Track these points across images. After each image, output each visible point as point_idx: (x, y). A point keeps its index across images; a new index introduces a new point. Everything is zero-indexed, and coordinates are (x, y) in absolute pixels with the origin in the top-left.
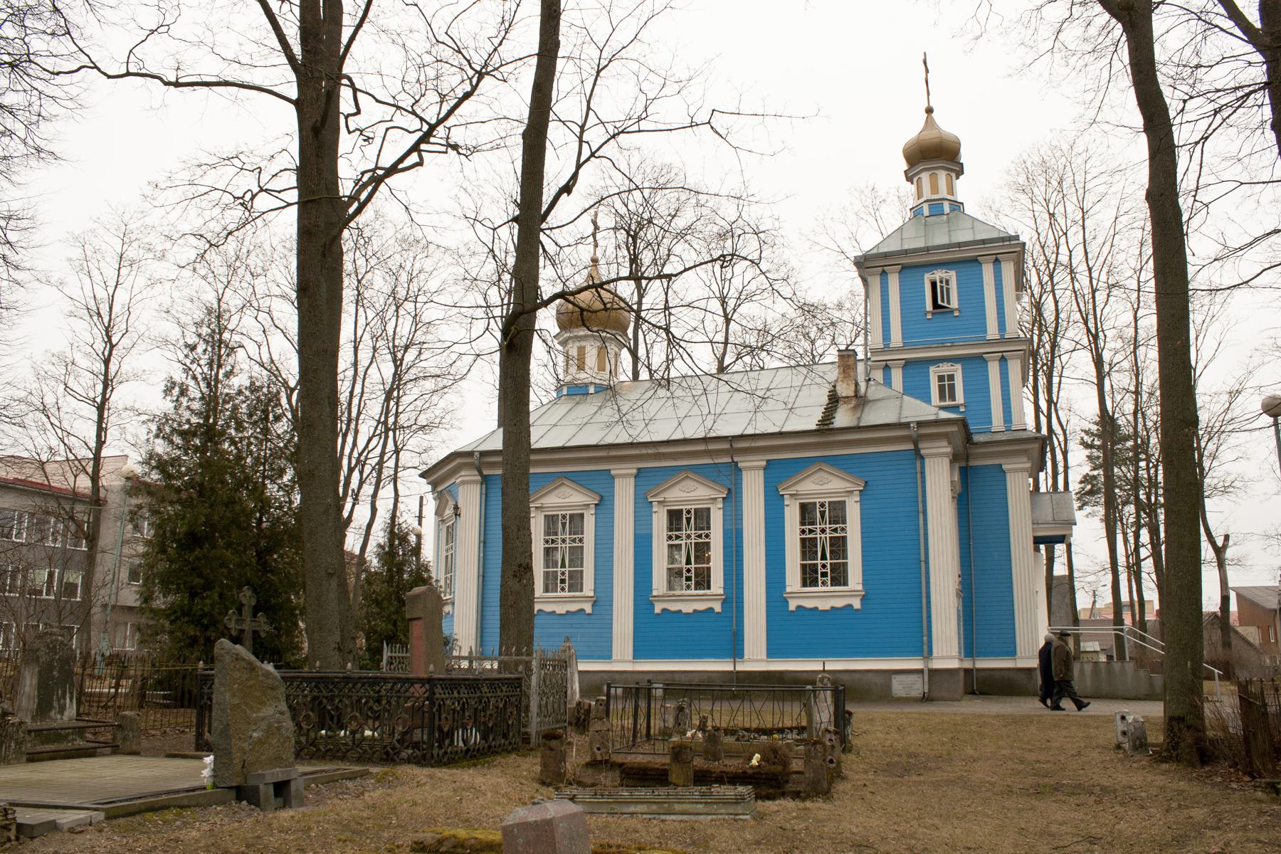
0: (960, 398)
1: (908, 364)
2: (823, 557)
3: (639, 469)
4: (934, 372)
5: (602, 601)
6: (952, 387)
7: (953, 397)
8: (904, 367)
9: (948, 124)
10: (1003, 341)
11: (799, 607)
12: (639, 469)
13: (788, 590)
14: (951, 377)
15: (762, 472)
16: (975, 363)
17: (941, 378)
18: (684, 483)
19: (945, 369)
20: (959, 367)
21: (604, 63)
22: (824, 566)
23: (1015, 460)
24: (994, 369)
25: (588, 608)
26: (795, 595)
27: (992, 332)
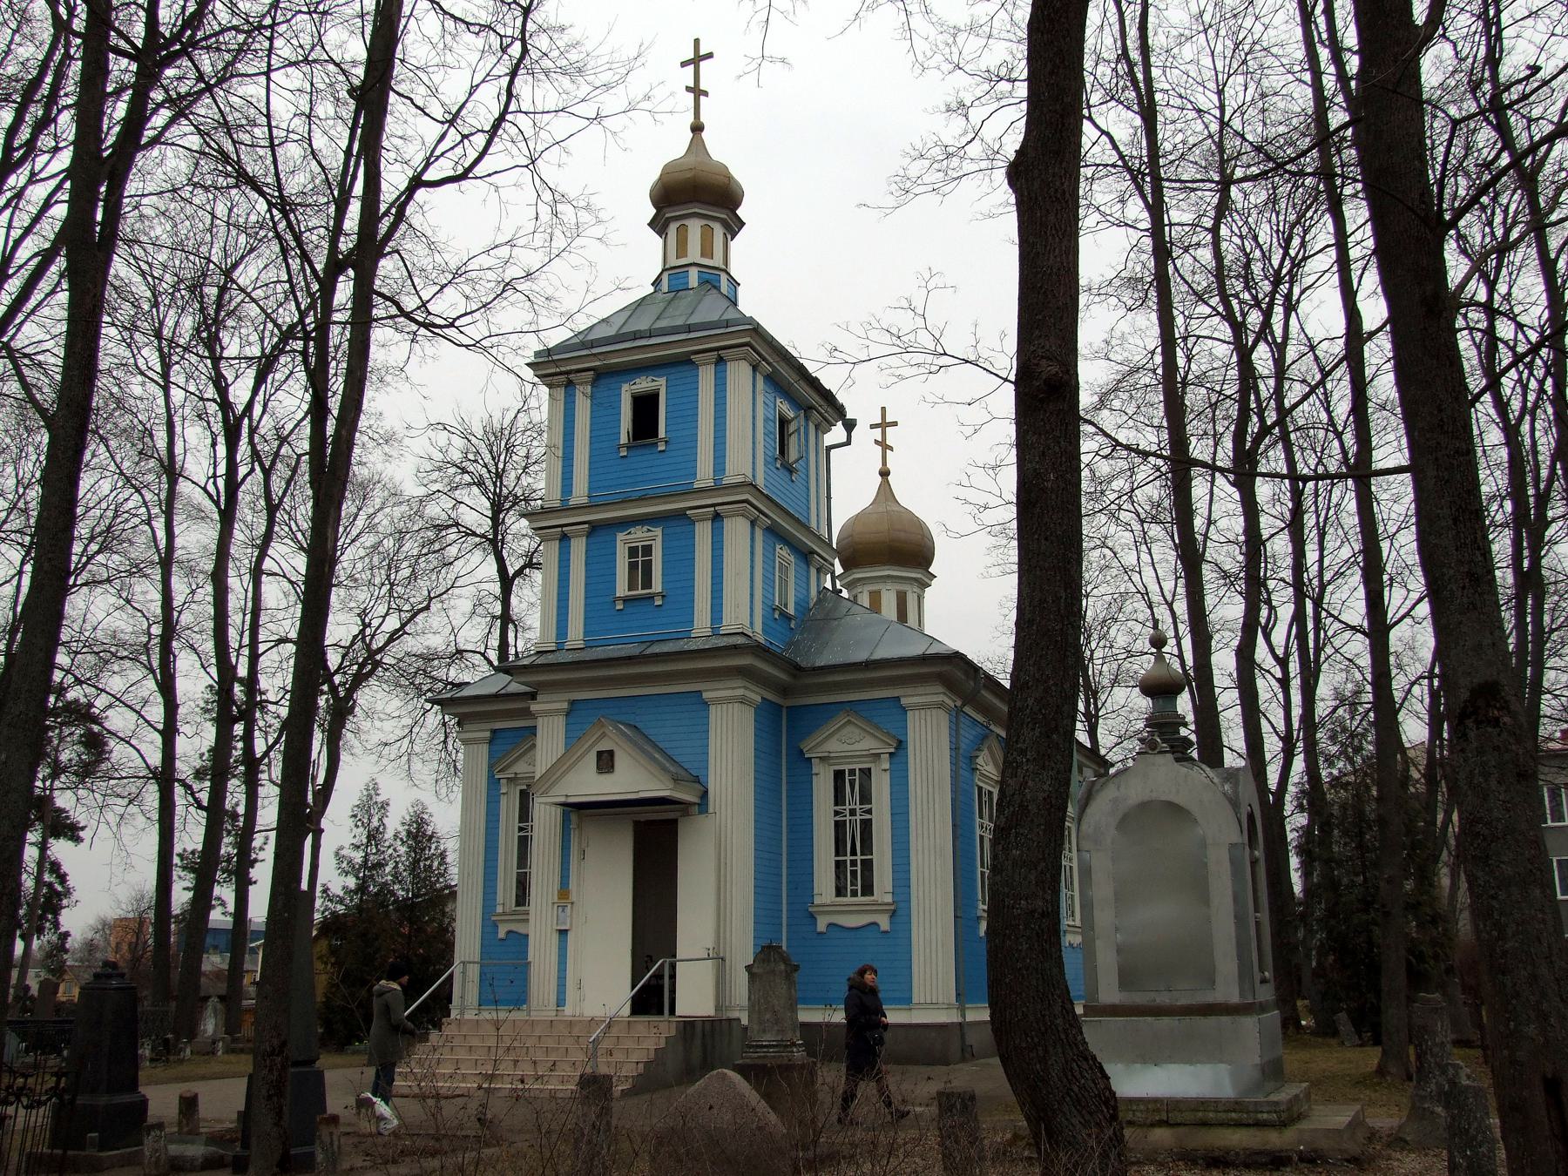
0: (657, 586)
1: (595, 528)
2: (854, 853)
3: (573, 703)
4: (622, 543)
5: (899, 911)
6: (648, 566)
7: (647, 583)
8: (589, 535)
9: (726, 150)
10: (718, 488)
11: (830, 925)
12: (573, 703)
13: (817, 901)
14: (648, 550)
15: (485, 748)
16: (678, 521)
17: (633, 552)
18: (845, 731)
19: (639, 535)
20: (658, 532)
21: (431, 175)
22: (854, 863)
23: (921, 690)
24: (703, 532)
25: (884, 922)
26: (828, 909)
27: (704, 474)
